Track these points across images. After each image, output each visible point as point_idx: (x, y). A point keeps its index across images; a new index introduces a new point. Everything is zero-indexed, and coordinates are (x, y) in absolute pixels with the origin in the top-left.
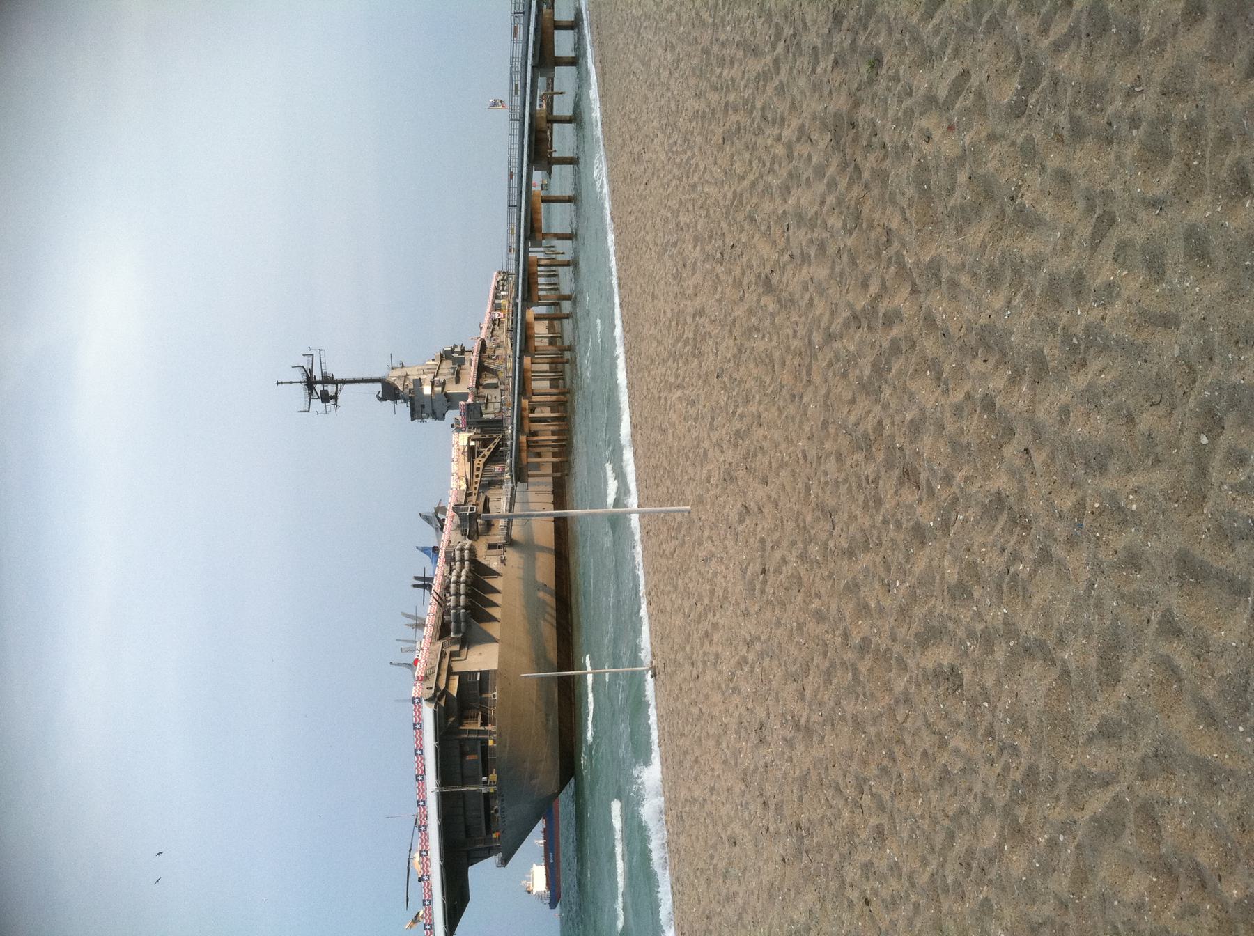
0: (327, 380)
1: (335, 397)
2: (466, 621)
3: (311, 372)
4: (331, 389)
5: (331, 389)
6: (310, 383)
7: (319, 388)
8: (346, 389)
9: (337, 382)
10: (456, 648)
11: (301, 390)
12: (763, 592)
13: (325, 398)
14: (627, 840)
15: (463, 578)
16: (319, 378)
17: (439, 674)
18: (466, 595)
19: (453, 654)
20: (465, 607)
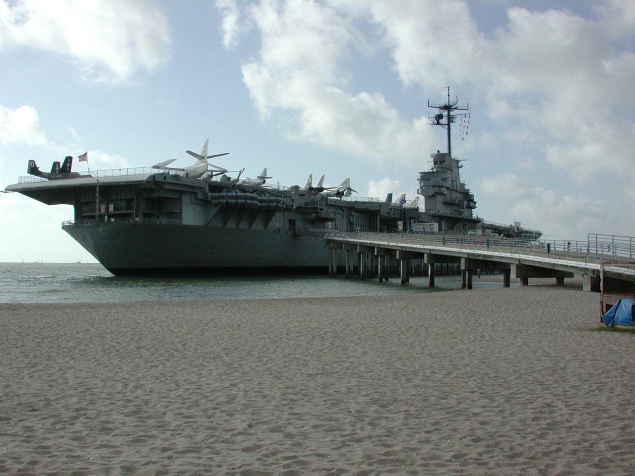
0: (450, 119)
1: (438, 123)
2: (219, 204)
3: (456, 108)
4: (444, 121)
5: (444, 121)
6: (448, 108)
7: (445, 113)
8: (445, 131)
9: (449, 125)
10: (200, 196)
11: (444, 102)
12: (498, 456)
13: (439, 117)
14: (386, 460)
15: (248, 201)
16: (452, 113)
17: (177, 185)
18: (269, 206)
19: (196, 194)
20: (227, 203)
